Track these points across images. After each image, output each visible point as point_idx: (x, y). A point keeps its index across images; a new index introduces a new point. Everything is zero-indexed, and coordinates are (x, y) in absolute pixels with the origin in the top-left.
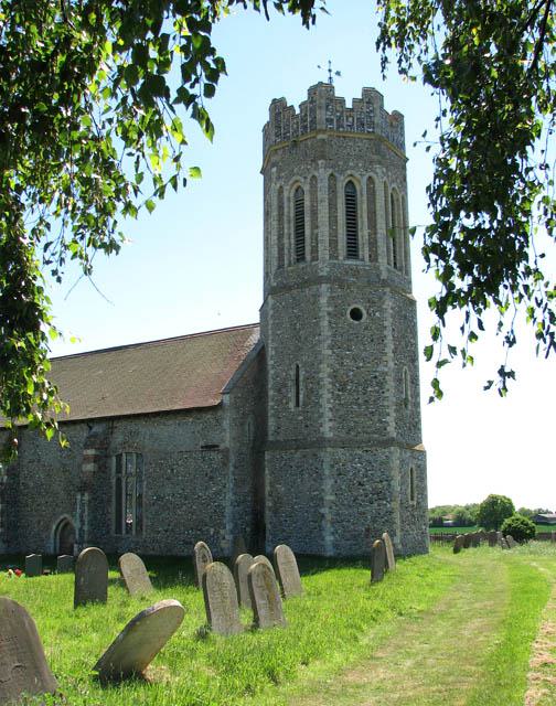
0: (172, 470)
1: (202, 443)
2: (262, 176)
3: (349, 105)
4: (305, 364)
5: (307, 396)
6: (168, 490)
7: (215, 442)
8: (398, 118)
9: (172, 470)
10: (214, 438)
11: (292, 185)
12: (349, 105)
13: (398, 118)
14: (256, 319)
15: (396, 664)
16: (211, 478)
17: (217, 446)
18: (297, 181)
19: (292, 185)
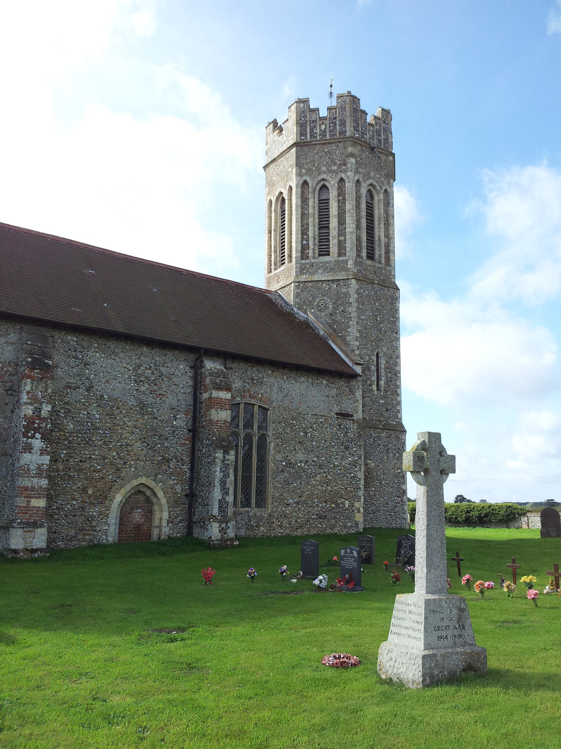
0: (306, 433)
1: (336, 409)
2: (450, 452)
3: (323, 113)
4: (385, 354)
5: (387, 383)
6: (301, 456)
7: (350, 411)
8: (453, 457)
9: (306, 433)
10: (347, 406)
11: (319, 182)
12: (369, 119)
13: (453, 457)
14: (393, 151)
15: (395, 716)
16: (347, 448)
17: (352, 416)
18: (323, 180)
19: (319, 182)
